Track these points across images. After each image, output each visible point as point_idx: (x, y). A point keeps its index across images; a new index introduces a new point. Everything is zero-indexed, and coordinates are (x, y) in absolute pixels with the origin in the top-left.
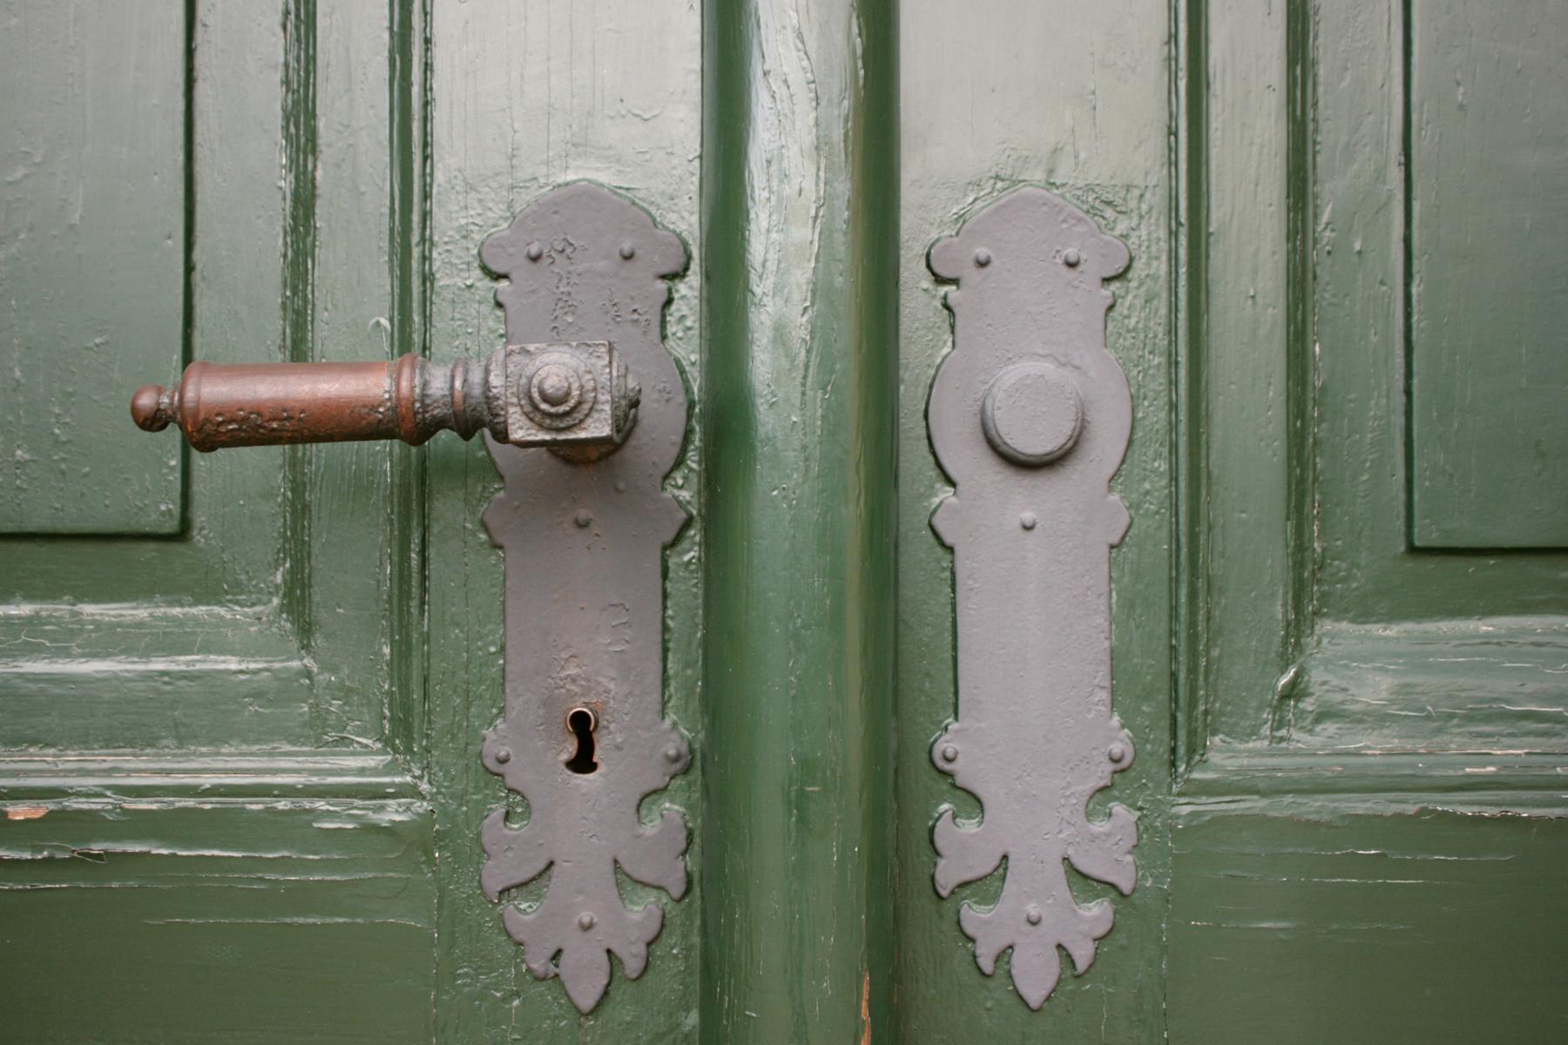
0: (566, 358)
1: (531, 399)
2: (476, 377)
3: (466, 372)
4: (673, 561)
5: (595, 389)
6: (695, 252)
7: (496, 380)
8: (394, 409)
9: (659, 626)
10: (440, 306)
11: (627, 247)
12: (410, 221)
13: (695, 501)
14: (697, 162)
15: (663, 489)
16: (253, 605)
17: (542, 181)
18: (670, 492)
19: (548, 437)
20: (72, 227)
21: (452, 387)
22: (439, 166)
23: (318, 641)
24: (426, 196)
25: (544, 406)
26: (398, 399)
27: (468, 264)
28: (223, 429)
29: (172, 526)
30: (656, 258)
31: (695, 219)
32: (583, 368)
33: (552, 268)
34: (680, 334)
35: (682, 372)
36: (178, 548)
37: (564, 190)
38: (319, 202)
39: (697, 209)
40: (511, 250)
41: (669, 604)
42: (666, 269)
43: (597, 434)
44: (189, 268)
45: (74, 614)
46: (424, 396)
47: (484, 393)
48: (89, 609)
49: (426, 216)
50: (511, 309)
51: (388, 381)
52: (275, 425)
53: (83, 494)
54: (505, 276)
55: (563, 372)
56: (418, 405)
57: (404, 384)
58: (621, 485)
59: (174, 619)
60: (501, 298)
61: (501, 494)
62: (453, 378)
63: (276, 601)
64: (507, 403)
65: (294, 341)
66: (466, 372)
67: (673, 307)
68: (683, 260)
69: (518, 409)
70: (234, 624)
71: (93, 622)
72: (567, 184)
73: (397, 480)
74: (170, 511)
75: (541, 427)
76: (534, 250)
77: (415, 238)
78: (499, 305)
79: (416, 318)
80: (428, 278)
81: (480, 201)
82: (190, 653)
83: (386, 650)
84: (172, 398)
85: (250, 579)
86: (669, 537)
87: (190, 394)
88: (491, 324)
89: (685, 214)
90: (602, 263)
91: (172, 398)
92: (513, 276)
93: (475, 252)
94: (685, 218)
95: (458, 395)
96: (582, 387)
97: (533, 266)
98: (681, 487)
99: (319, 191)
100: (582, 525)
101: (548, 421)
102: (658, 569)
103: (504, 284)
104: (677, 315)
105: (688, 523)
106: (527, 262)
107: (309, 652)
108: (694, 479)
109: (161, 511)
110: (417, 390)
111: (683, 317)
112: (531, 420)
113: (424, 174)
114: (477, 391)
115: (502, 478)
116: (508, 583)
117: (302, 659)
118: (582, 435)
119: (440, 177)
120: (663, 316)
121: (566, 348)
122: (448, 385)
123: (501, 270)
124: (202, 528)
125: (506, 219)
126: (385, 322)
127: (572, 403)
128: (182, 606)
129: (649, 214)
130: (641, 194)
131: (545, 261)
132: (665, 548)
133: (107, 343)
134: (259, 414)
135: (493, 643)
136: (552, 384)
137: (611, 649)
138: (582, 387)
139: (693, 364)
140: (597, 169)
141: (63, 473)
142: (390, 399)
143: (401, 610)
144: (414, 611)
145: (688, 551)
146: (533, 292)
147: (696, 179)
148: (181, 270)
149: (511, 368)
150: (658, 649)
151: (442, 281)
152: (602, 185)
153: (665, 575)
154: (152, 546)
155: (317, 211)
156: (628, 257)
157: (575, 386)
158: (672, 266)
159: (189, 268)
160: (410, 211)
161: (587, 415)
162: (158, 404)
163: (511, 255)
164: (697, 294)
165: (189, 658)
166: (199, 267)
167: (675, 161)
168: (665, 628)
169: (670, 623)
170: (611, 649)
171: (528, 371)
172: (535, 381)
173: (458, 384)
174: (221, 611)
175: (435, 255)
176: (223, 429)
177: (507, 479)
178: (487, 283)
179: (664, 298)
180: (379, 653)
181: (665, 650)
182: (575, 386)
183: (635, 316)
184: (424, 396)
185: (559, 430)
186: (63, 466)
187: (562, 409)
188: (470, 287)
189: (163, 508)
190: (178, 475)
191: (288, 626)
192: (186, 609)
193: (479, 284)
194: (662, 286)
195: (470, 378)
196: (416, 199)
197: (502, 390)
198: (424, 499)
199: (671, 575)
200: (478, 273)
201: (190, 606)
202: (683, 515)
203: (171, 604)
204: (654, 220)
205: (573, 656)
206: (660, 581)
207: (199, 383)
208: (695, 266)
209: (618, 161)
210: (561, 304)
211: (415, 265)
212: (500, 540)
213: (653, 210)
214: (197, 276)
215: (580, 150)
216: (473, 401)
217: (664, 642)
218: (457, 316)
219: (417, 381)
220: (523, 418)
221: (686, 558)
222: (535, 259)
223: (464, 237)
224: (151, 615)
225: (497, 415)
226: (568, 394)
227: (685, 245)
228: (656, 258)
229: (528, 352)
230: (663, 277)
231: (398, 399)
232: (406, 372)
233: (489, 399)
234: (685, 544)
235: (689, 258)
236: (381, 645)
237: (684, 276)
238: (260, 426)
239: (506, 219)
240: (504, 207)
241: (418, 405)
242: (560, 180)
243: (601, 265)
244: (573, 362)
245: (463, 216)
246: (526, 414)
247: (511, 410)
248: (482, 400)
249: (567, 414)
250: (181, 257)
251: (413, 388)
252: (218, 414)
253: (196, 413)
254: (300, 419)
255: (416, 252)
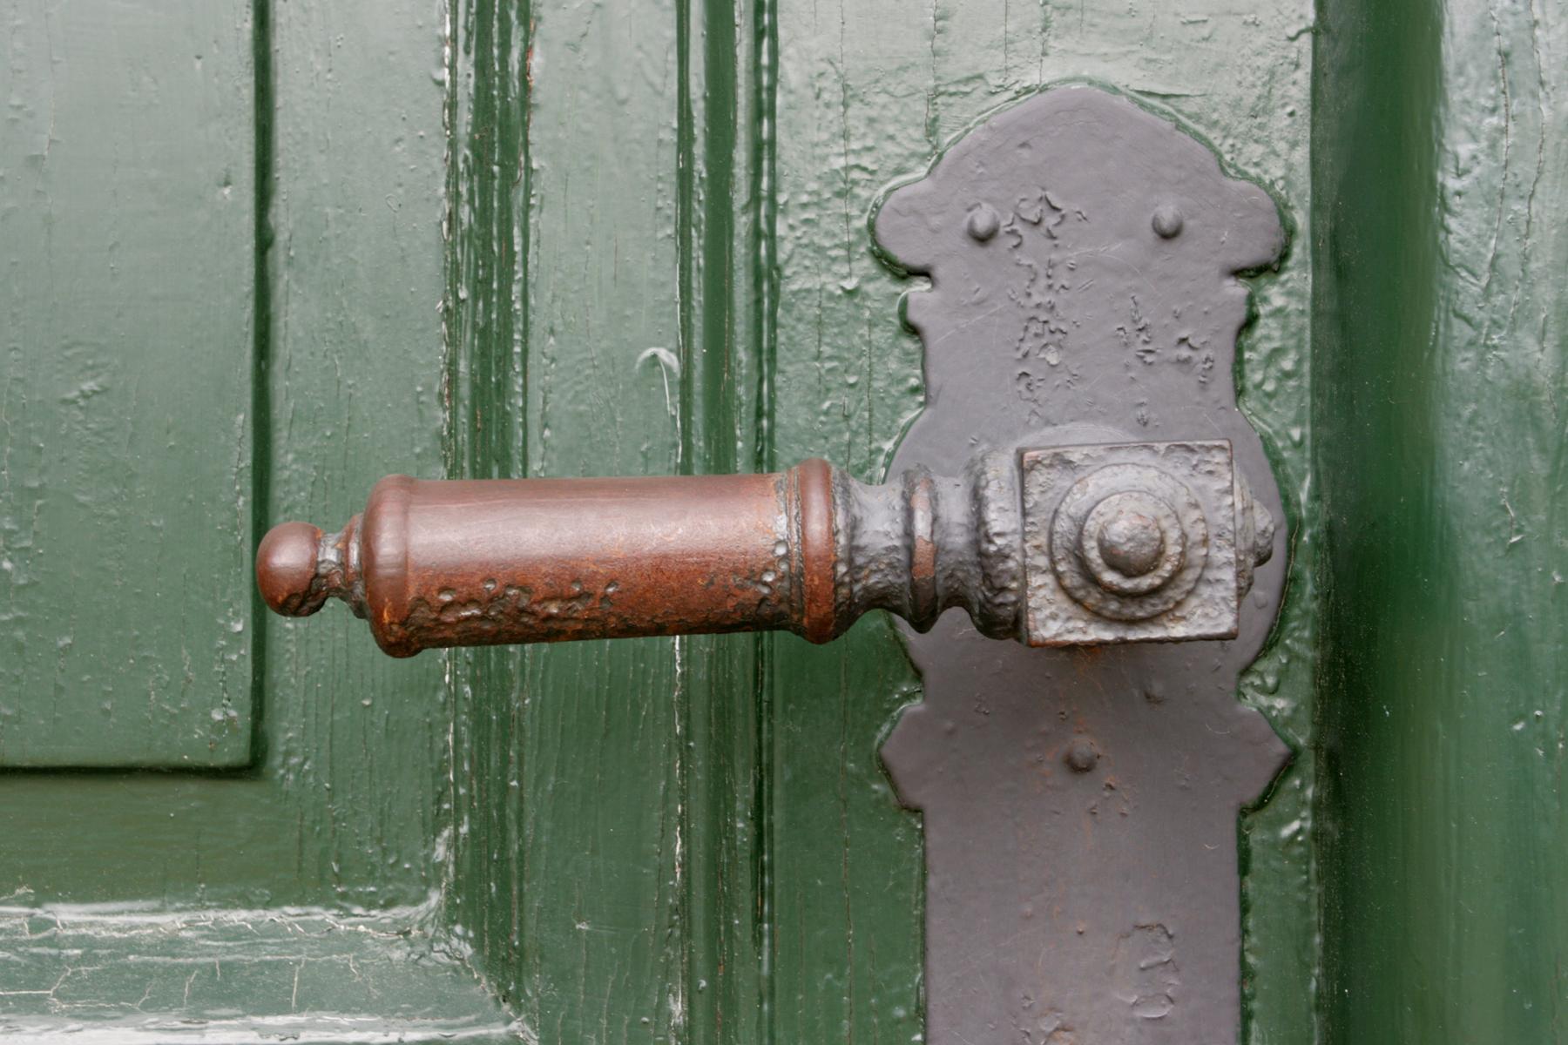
0: (1150, 478)
1: (1082, 564)
2: (956, 509)
3: (934, 500)
4: (1257, 837)
5: (1205, 542)
6: (1301, 219)
7: (1001, 519)
8: (795, 578)
9: (1234, 970)
10: (793, 330)
11: (1167, 214)
12: (729, 161)
13: (1305, 716)
14: (1306, 41)
15: (1241, 695)
16: (387, 905)
17: (994, 80)
18: (1253, 702)
19: (1108, 636)
20: (35, 161)
21: (909, 533)
22: (787, 52)
23: (535, 985)
24: (763, 109)
25: (1110, 577)
26: (805, 558)
27: (849, 247)
28: (449, 617)
29: (233, 751)
30: (1225, 236)
31: (1301, 155)
32: (1183, 499)
33: (1017, 256)
34: (1269, 387)
35: (1276, 462)
36: (241, 791)
37: (1036, 100)
38: (536, 119)
39: (1305, 134)
40: (936, 221)
41: (1251, 923)
42: (1245, 258)
43: (1208, 629)
44: (264, 242)
45: (38, 925)
46: (853, 549)
47: (976, 543)
48: (67, 915)
49: (763, 149)
50: (935, 341)
51: (782, 520)
52: (554, 610)
53: (59, 690)
54: (925, 273)
55: (1148, 509)
56: (842, 569)
57: (817, 528)
58: (1158, 688)
59: (236, 934)
60: (915, 316)
61: (916, 705)
62: (909, 513)
63: (435, 898)
64: (1025, 569)
65: (479, 391)
66: (934, 500)
67: (1259, 332)
68: (1278, 240)
69: (1049, 579)
70: (353, 942)
71: (79, 941)
72: (1043, 89)
73: (701, 674)
74: (231, 721)
75: (1097, 615)
76: (982, 224)
77: (740, 197)
78: (912, 330)
79: (743, 355)
80: (766, 274)
81: (871, 121)
82: (284, 1009)
83: (677, 1007)
84: (345, 552)
85: (385, 852)
86: (1251, 794)
87: (387, 548)
88: (893, 365)
89: (1282, 147)
90: (1118, 246)
91: (345, 552)
92: (939, 272)
93: (861, 223)
94: (1282, 156)
95: (923, 548)
96: (1184, 536)
97: (980, 253)
98: (1274, 692)
99: (537, 98)
100: (1078, 768)
101: (1114, 605)
102: (1232, 857)
103: (919, 287)
104: (1266, 347)
105: (1289, 765)
106: (967, 245)
107: (519, 1008)
108: (1304, 677)
109: (215, 727)
110: (842, 540)
111: (1277, 353)
112: (1077, 601)
113: (757, 68)
114: (958, 539)
115: (918, 675)
116: (932, 882)
117: (508, 1021)
118: (1179, 631)
119: (791, 71)
120: (1239, 351)
121: (1145, 456)
122: (899, 529)
123: (917, 261)
124: (288, 754)
125: (924, 157)
126: (669, 358)
127: (1167, 568)
128: (250, 906)
129: (1209, 145)
130: (1190, 107)
131: (1004, 243)
132: (1244, 812)
133: (104, 391)
134: (524, 589)
135: (901, 1000)
136: (1122, 525)
137: (1140, 1014)
138: (1184, 536)
139: (1298, 445)
140: (1105, 57)
141: (20, 648)
142: (786, 558)
143: (712, 935)
144: (744, 934)
145: (1287, 821)
146: (979, 303)
147: (1303, 76)
148: (249, 247)
149: (1035, 495)
150: (1231, 1014)
151: (796, 282)
152: (1115, 90)
153: (1244, 868)
154: (192, 787)
155: (533, 136)
156: (1169, 236)
157: (1173, 535)
158: (1255, 251)
159: (264, 242)
160: (730, 143)
161: (1190, 593)
162: (315, 563)
163: (935, 231)
164: (1307, 306)
165: (281, 1020)
166: (281, 238)
167: (1260, 40)
168: (1246, 973)
169: (1251, 959)
170: (1140, 1014)
171: (1075, 504)
172: (1091, 526)
173: (922, 526)
174: (329, 916)
175: (781, 229)
176: (449, 617)
177: (930, 676)
178: (885, 285)
179: (1240, 315)
180: (661, 1011)
181: (1246, 1017)
182: (1173, 535)
183: (1184, 352)
184: (853, 549)
185: (1132, 622)
186: (20, 634)
187: (1145, 582)
188: (851, 293)
189: (217, 716)
190: (246, 650)
191: (468, 950)
192: (258, 914)
193: (869, 288)
194: (1237, 290)
195: (943, 511)
196: (742, 118)
197: (1016, 541)
198: (762, 711)
199: (1255, 865)
200: (866, 265)
201: (267, 906)
202: (1279, 749)
203: (226, 904)
204: (1219, 156)
205: (1063, 1028)
206: (1235, 879)
207: (404, 526)
208: (1300, 250)
209: (1147, 40)
210: (1035, 328)
211: (740, 249)
212: (916, 796)
213: (1214, 136)
214: (278, 255)
215: (1071, 17)
216: (949, 560)
217: (1244, 999)
218: (827, 350)
219: (840, 520)
220: (1060, 597)
221: (1286, 832)
222: (983, 239)
223: (839, 194)
224: (190, 925)
225: (1003, 589)
226: (1159, 554)
227: (1282, 209)
228: (1225, 236)
229: (1068, 464)
230: (1238, 273)
231: (805, 558)
232: (817, 500)
233: (984, 558)
234: (1281, 804)
235: (1290, 232)
236: (664, 994)
237: (1278, 272)
238: (522, 611)
239: (924, 157)
240: (918, 134)
241: (842, 569)
242: (1032, 79)
243: (1116, 249)
244: (1165, 487)
245: (833, 149)
246: (1068, 592)
247: (1036, 580)
248: (970, 556)
249: (1154, 591)
250: (248, 220)
251: (833, 533)
252: (444, 589)
253: (401, 583)
254: (605, 597)
255: (742, 224)
